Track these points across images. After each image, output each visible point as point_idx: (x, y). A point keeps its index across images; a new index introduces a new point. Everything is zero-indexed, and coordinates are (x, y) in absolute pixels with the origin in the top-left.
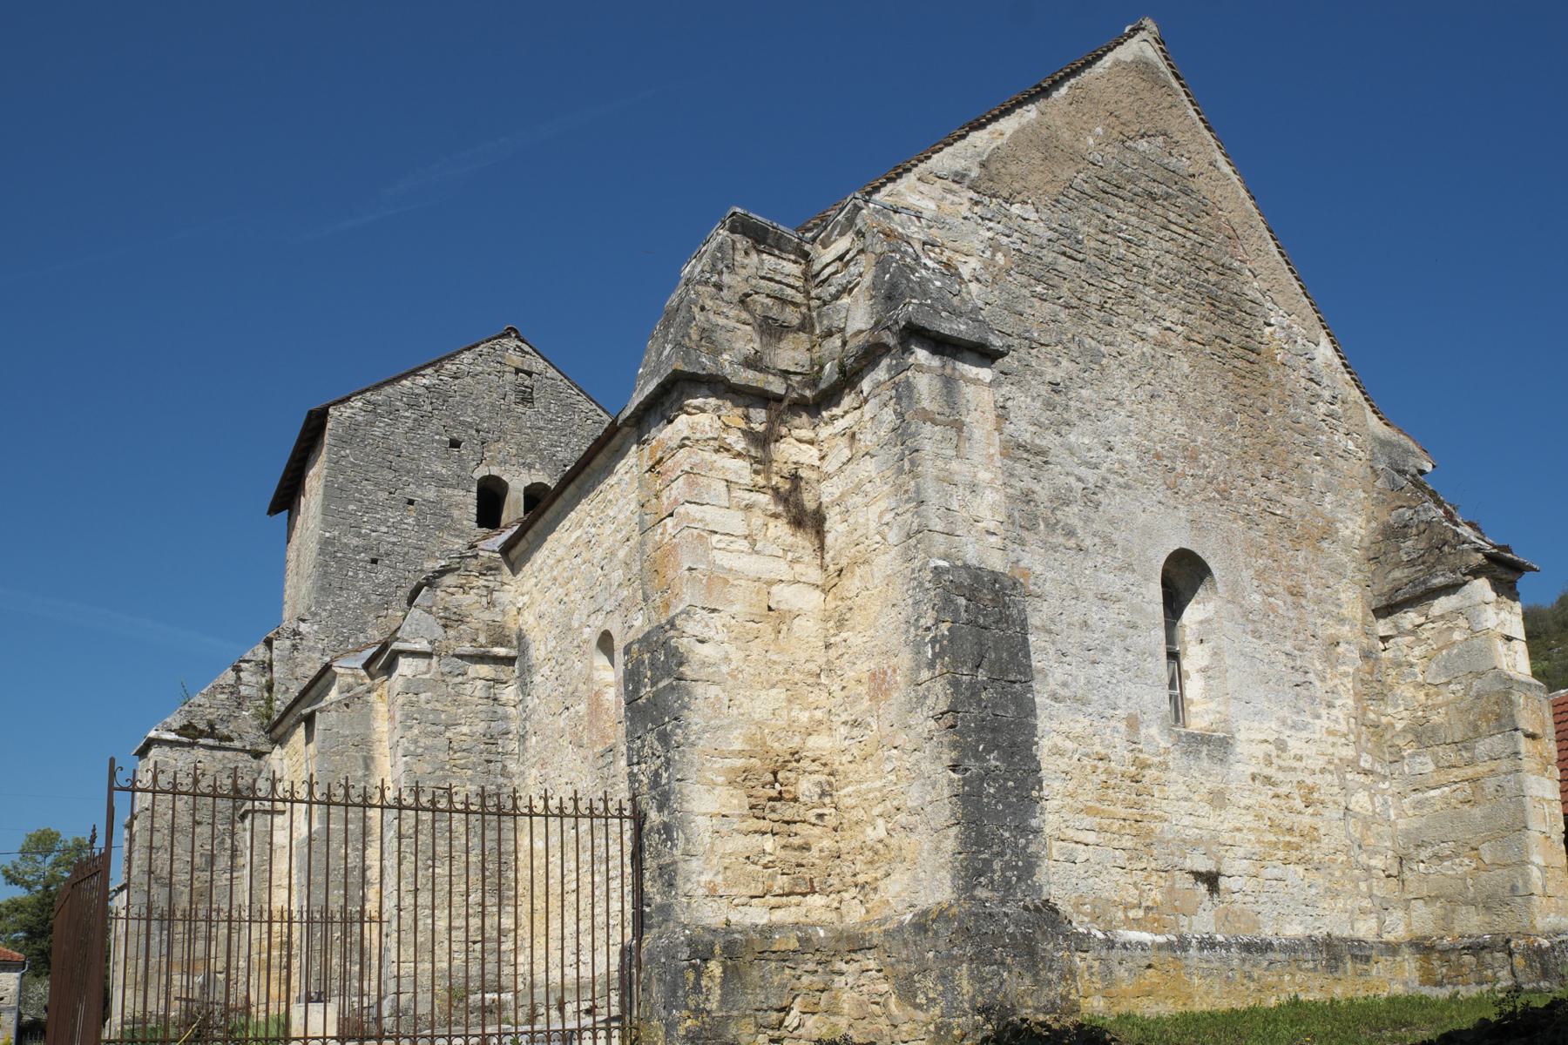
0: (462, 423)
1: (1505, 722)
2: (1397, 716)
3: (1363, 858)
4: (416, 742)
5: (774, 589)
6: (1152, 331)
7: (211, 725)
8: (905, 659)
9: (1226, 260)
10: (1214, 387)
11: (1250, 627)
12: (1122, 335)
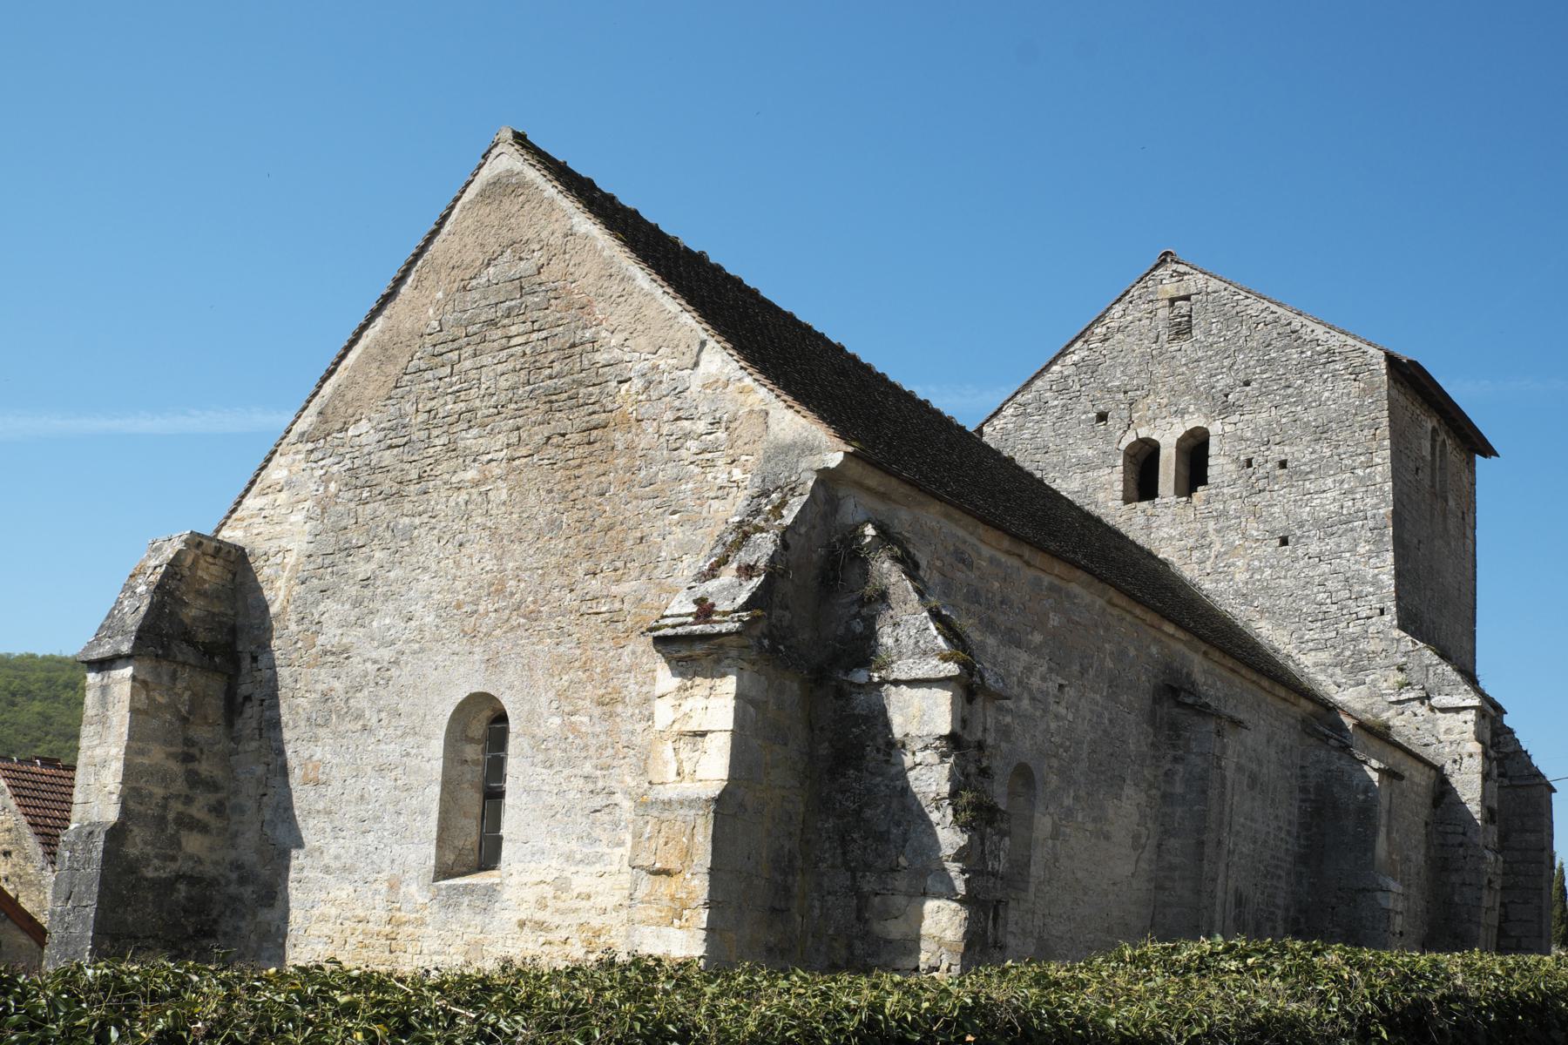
11: (541, 757)
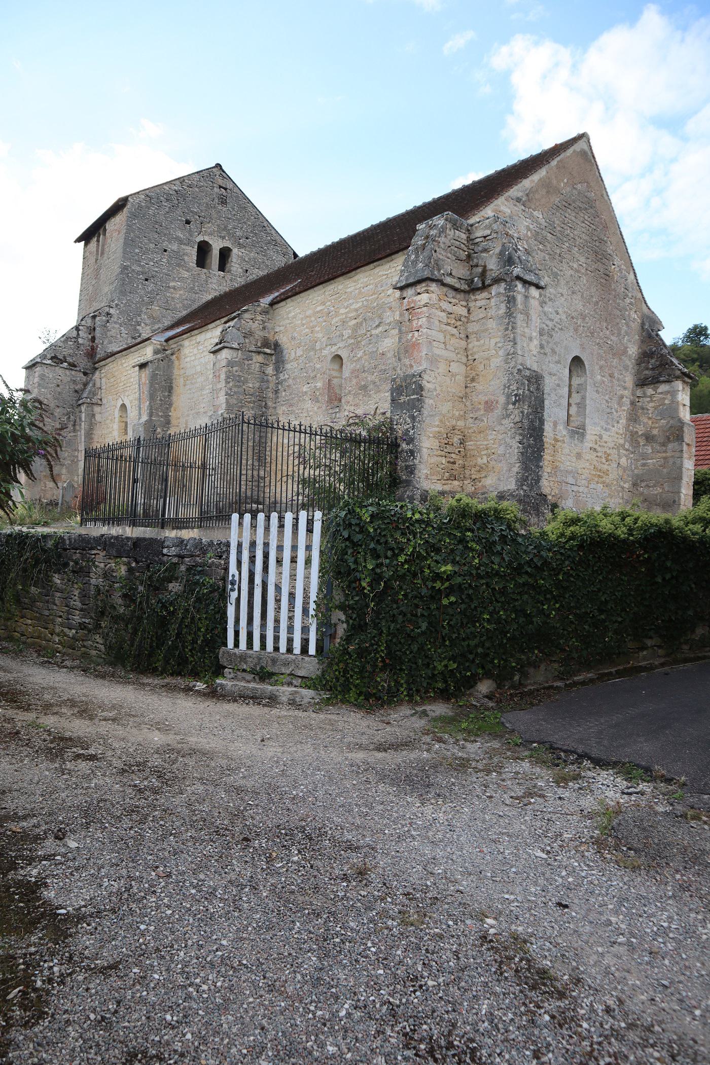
0: (192, 212)
1: (680, 438)
2: (641, 430)
3: (622, 484)
4: (231, 389)
6: (575, 266)
7: (64, 357)
8: (502, 399)
9: (602, 237)
10: (593, 290)
12: (565, 266)
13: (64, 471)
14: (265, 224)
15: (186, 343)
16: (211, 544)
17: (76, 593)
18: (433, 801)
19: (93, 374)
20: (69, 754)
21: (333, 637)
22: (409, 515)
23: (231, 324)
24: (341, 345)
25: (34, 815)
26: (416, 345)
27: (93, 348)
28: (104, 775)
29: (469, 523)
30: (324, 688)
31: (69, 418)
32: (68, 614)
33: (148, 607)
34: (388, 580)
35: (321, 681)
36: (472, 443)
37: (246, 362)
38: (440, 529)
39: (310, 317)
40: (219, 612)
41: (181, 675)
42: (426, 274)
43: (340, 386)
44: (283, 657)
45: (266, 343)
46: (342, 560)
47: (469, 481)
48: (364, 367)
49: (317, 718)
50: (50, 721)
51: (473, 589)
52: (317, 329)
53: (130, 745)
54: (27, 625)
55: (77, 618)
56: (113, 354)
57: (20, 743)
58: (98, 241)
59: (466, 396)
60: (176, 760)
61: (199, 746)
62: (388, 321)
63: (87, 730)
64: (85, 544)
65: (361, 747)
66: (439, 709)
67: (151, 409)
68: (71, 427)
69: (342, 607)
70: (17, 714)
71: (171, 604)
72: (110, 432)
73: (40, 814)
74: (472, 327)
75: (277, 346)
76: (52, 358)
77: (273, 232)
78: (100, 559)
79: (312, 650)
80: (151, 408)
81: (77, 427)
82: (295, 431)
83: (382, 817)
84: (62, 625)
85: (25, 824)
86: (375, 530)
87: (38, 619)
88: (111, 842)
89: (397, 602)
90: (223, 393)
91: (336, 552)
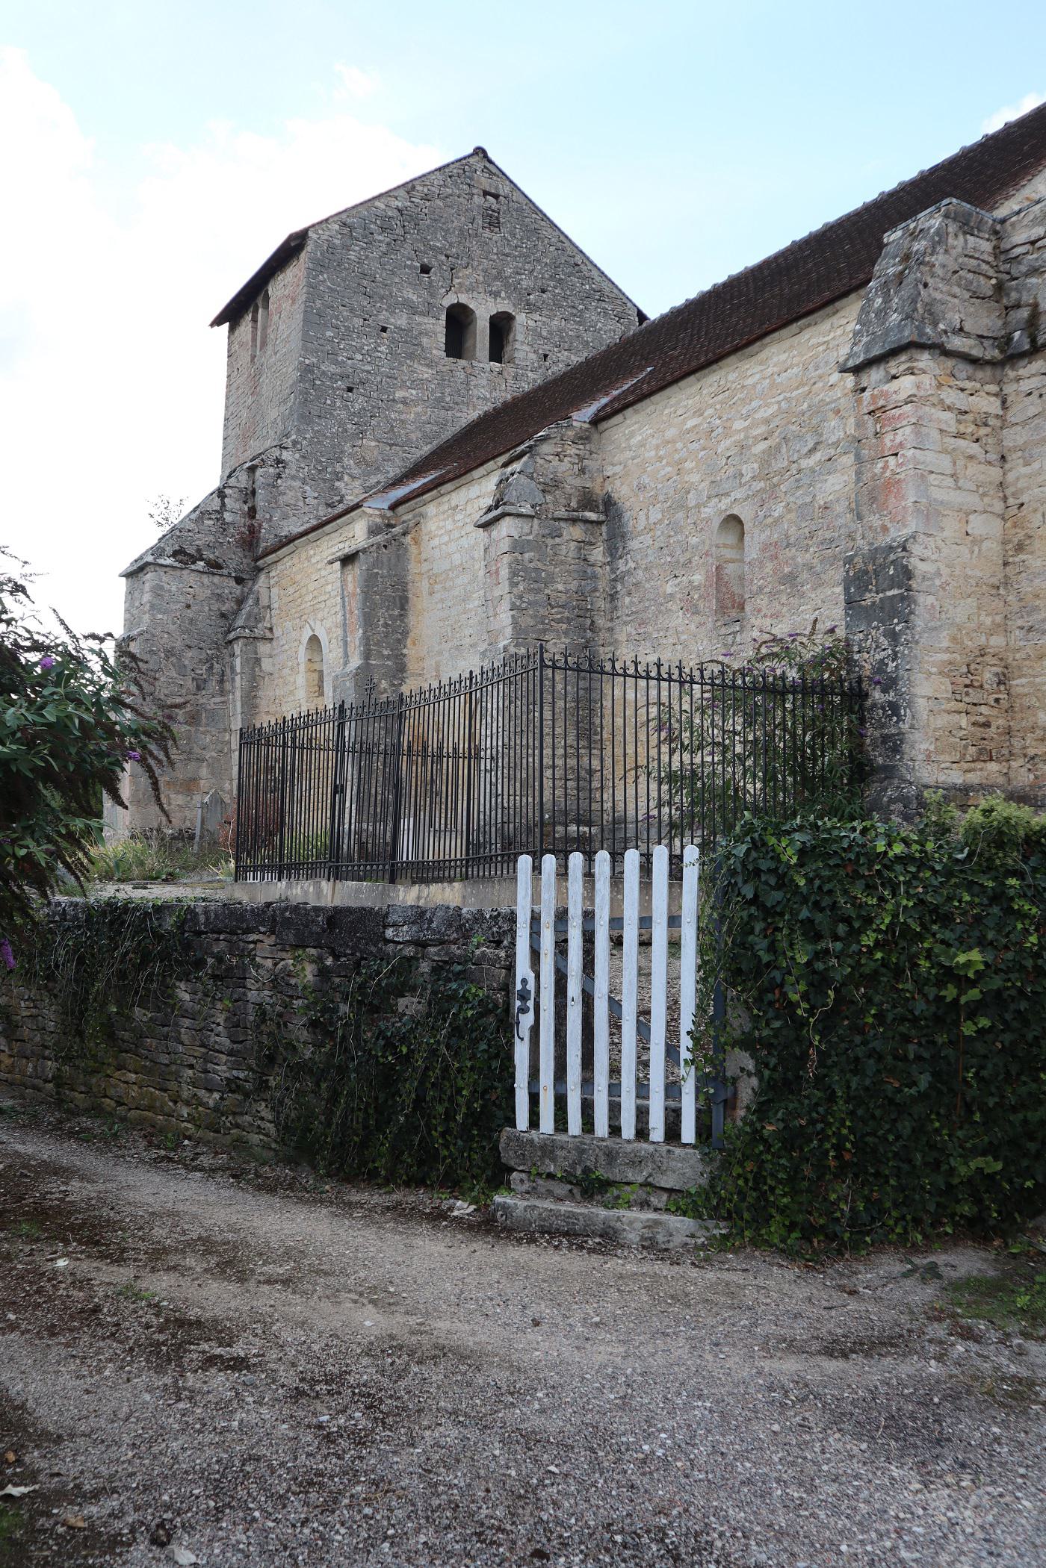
0: (432, 248)
4: (521, 597)
5: (971, 517)
7: (199, 550)
13: (204, 772)
14: (578, 259)
15: (431, 509)
16: (478, 917)
17: (221, 1019)
18: (950, 1479)
19: (254, 579)
20: (193, 1356)
21: (730, 1104)
22: (881, 846)
23: (517, 466)
24: (738, 494)
25: (114, 1491)
26: (892, 485)
27: (253, 531)
28: (259, 1402)
29: (1013, 858)
30: (715, 1213)
31: (211, 667)
32: (206, 1061)
33: (358, 1047)
34: (843, 984)
35: (708, 1199)
36: (1023, 680)
37: (550, 541)
38: (949, 873)
39: (674, 441)
40: (497, 1056)
41: (426, 1186)
42: (908, 334)
43: (741, 578)
44: (629, 1148)
45: (588, 501)
46: (743, 945)
47: (1021, 762)
48: (787, 537)
49: (698, 1279)
50: (160, 1284)
51: (1028, 998)
52: (689, 465)
53: (315, 1335)
54: (128, 1083)
55: (222, 1070)
56: (291, 540)
57: (100, 1332)
58: (254, 320)
59: (1006, 582)
60: (406, 1369)
61: (454, 1341)
62: (834, 439)
63: (233, 1304)
64: (236, 922)
65: (792, 1347)
66: (966, 1262)
67: (367, 644)
68: (213, 685)
69: (747, 1043)
70: (99, 1269)
71: (403, 1039)
72: (291, 693)
73: (127, 1488)
74: (1013, 437)
75: (609, 506)
76: (175, 554)
77: (595, 273)
78: (264, 948)
79: (688, 1134)
80: (366, 640)
81: (228, 686)
82: (648, 678)
83: (836, 1511)
84: (193, 1083)
85: (94, 1509)
86: (810, 881)
87: (149, 1072)
88: (262, 1553)
89: (861, 1031)
90: (505, 605)
91: (729, 932)
